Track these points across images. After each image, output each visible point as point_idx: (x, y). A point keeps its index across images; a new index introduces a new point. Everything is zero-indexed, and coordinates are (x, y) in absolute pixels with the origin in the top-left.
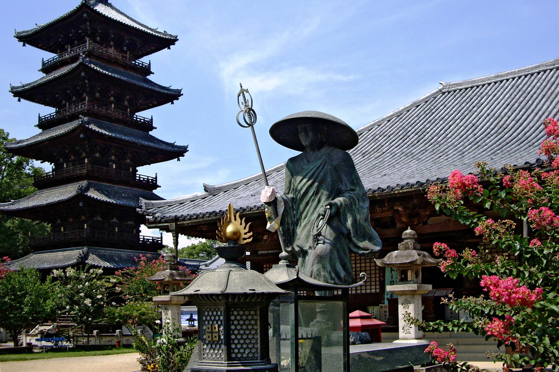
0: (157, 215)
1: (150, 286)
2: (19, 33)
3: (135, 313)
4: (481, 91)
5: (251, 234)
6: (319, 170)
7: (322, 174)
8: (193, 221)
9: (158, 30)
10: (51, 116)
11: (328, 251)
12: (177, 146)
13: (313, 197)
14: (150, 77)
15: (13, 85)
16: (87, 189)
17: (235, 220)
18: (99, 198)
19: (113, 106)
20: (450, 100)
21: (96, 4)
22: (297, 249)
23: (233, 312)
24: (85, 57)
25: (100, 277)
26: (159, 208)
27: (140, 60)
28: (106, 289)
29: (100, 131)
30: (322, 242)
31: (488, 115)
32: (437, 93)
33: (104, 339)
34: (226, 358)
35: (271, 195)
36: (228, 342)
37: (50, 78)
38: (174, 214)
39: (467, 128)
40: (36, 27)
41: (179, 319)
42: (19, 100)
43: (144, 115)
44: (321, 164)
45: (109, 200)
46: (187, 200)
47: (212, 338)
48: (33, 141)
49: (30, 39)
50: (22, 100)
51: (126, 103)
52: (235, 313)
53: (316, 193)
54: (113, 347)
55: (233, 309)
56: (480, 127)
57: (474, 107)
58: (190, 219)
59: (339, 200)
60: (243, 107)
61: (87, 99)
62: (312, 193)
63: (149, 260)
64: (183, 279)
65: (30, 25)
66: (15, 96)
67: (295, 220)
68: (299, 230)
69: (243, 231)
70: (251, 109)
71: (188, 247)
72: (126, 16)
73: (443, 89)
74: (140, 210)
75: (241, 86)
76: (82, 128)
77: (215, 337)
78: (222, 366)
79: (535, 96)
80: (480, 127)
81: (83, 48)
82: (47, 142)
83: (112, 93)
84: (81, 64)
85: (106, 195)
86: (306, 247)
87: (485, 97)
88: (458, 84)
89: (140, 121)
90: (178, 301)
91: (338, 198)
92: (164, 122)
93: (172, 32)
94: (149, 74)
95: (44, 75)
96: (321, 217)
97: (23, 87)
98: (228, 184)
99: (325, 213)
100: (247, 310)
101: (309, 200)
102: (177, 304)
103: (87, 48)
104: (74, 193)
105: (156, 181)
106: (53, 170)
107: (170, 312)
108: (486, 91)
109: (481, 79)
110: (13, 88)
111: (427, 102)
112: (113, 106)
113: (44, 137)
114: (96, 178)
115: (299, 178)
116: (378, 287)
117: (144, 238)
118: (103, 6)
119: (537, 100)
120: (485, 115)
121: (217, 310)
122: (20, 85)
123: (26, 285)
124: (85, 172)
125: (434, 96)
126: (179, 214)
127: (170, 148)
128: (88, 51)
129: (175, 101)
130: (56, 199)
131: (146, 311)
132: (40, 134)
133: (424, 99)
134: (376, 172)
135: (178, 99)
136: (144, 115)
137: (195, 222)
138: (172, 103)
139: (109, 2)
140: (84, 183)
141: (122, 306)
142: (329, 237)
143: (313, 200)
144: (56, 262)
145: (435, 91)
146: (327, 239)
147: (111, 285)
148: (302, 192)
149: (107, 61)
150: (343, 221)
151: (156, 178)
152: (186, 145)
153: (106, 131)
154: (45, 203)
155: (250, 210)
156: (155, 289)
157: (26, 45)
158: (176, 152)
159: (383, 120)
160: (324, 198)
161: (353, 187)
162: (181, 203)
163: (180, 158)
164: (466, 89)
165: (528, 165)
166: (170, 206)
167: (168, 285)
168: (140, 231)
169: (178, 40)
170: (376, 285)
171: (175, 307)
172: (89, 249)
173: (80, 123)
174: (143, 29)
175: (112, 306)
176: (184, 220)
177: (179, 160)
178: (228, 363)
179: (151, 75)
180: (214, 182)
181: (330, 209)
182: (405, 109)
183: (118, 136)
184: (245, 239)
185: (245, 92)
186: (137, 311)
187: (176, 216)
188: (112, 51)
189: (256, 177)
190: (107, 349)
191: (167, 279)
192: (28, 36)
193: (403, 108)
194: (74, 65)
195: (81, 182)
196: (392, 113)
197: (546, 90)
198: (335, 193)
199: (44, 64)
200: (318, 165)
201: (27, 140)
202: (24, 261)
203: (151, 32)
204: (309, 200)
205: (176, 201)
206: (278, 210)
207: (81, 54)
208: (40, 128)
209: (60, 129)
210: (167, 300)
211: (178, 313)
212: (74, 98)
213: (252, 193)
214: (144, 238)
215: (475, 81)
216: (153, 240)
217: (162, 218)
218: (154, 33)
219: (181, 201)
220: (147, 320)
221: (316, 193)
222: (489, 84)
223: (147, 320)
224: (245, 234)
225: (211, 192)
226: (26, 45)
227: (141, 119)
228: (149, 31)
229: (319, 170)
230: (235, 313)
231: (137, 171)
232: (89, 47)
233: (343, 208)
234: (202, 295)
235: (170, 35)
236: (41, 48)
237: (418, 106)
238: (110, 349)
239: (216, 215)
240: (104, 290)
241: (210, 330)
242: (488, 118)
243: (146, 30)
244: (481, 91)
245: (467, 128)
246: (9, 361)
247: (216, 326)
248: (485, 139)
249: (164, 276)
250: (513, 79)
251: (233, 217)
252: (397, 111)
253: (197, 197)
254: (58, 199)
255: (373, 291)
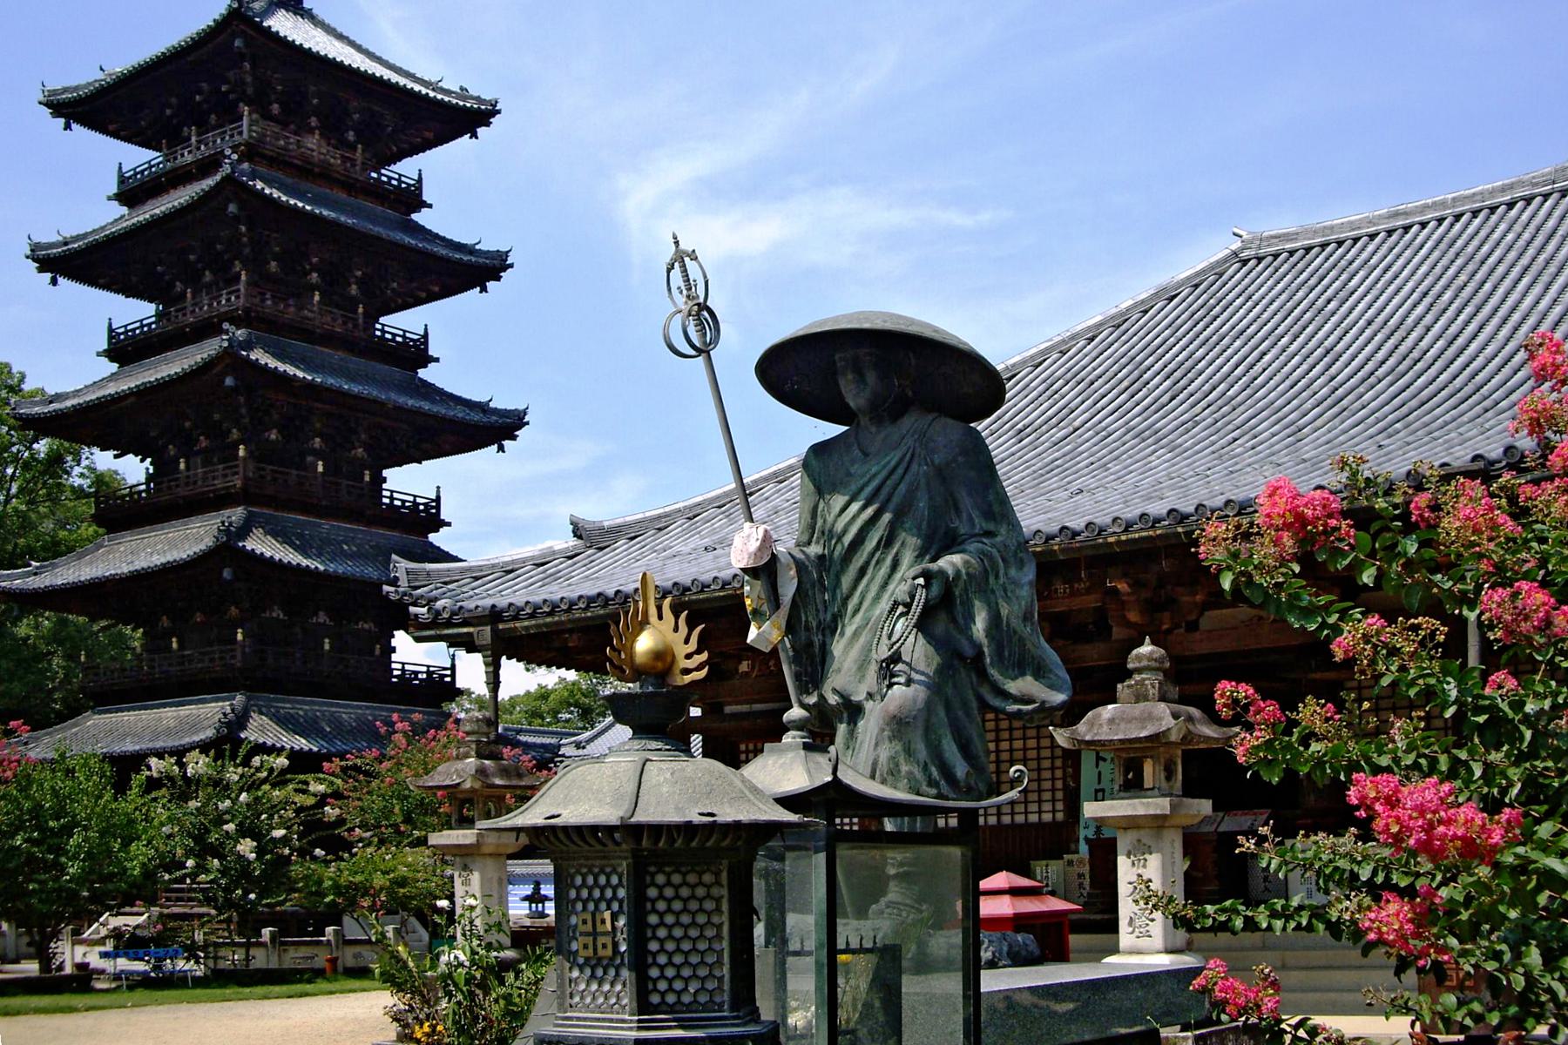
0: (439, 604)
1: (422, 803)
2: (54, 92)
3: (379, 880)
4: (1349, 256)
5: (704, 656)
6: (896, 477)
7: (903, 488)
8: (541, 621)
9: (443, 85)
10: (142, 326)
11: (920, 704)
12: (496, 411)
13: (878, 555)
14: (421, 217)
15: (36, 239)
16: (244, 531)
17: (660, 617)
18: (277, 557)
19: (317, 298)
20: (1263, 282)
21: (268, 12)
22: (833, 699)
23: (653, 875)
24: (240, 161)
25: (279, 779)
26: (446, 583)
27: (393, 167)
28: (298, 811)
29: (282, 367)
30: (902, 680)
31: (1369, 323)
32: (1225, 260)
33: (292, 952)
34: (635, 1004)
35: (760, 549)
36: (640, 961)
37: (141, 218)
38: (488, 602)
39: (1310, 361)
40: (101, 76)
41: (501, 897)
42: (54, 282)
43: (403, 322)
44: (901, 460)
45: (305, 562)
46: (524, 561)
47: (595, 950)
48: (94, 397)
49: (84, 109)
50: (60, 280)
51: (354, 289)
52: (660, 879)
53: (887, 542)
54: (316, 974)
55: (652, 869)
56: (1345, 357)
57: (1329, 301)
58: (532, 616)
59: (951, 562)
60: (681, 300)
61: (243, 278)
62: (874, 543)
63: (418, 731)
64: (514, 782)
65: (85, 70)
66: (41, 270)
67: (829, 617)
68: (837, 647)
69: (681, 650)
70: (703, 307)
71: (528, 693)
72: (352, 44)
73: (1243, 249)
74: (392, 589)
75: (677, 243)
76: (230, 359)
77: (604, 946)
78: (622, 1029)
79: (1501, 269)
80: (1345, 357)
81: (232, 136)
82: (132, 399)
83: (315, 260)
84: (227, 179)
85: (296, 548)
86: (857, 693)
87: (1362, 273)
88: (1284, 235)
89: (393, 340)
90: (498, 846)
91: (948, 557)
92: (460, 342)
93: (482, 90)
94: (417, 209)
95: (125, 210)
96: (901, 609)
97: (66, 244)
98: (640, 516)
99: (912, 597)
100: (693, 871)
101: (867, 563)
102: (495, 855)
103: (245, 135)
104: (207, 542)
105: (438, 507)
106: (150, 478)
107: (476, 877)
108: (1364, 255)
109: (1351, 223)
110: (35, 248)
111: (1196, 286)
112: (317, 298)
113: (125, 385)
114: (269, 500)
115: (839, 501)
116: (1060, 806)
117: (403, 670)
118: (290, 16)
119: (1507, 282)
120: (1362, 322)
121: (608, 870)
122: (55, 238)
123: (72, 801)
124: (239, 483)
125: (1218, 270)
126: (502, 602)
127: (476, 417)
128: (247, 144)
129: (490, 285)
130: (158, 560)
131: (410, 875)
132: (113, 377)
133: (1189, 278)
134: (1053, 482)
135: (498, 279)
136: (403, 322)
137: (546, 625)
138: (484, 289)
139: (307, 5)
140: (236, 514)
141: (343, 860)
142: (922, 667)
143: (878, 562)
144: (157, 737)
145: (1220, 255)
146: (917, 672)
147: (311, 801)
148: (847, 539)
149: (301, 172)
150: (961, 621)
151: (438, 500)
152: (521, 407)
153: (298, 367)
154: (125, 569)
155: (702, 591)
156: (435, 812)
157: (74, 126)
158: (493, 428)
159: (1073, 337)
160: (907, 557)
161: (991, 527)
162: (509, 570)
163: (506, 443)
164: (1308, 250)
165: (1481, 464)
166: (476, 579)
167: (470, 801)
168: (394, 650)
169: (499, 112)
170: (1054, 801)
171: (490, 862)
172: (249, 699)
173: (226, 344)
174: (402, 81)
175: (314, 859)
176: (516, 618)
177: (501, 449)
178: (639, 1021)
179: (424, 210)
180: (601, 511)
181: (927, 586)
182: (1136, 305)
183: (331, 381)
184: (687, 671)
185: (687, 259)
186: (385, 873)
187: (494, 606)
188: (313, 143)
189: (718, 497)
190: (300, 981)
191: (468, 785)
192: (79, 102)
193: (1130, 302)
194: (208, 183)
195: (227, 512)
196: (1099, 318)
197: (1531, 252)
198: (939, 541)
199: (122, 179)
200: (893, 463)
201: (77, 393)
202: (68, 733)
203: (424, 91)
204: (867, 563)
205: (493, 566)
206: (780, 591)
207: (228, 152)
208: (112, 360)
209: (168, 362)
210: (468, 842)
211: (500, 881)
212: (208, 276)
213: (707, 541)
214: (403, 670)
215: (1332, 228)
216: (429, 673)
217: (453, 613)
218: (432, 94)
219: (507, 563)
220: (413, 898)
221: (887, 542)
222: (1372, 237)
223: (413, 898)
224: (688, 656)
225: (592, 538)
226: (74, 126)
227: (394, 335)
228: (417, 88)
229: (896, 477)
230: (660, 879)
231: (384, 480)
232: (250, 131)
233: (961, 584)
234: (566, 829)
235: (478, 99)
236: (115, 135)
237: (1171, 299)
238: (309, 982)
239: (606, 605)
240: (291, 814)
241: (589, 927)
242: (1368, 332)
243: (410, 85)
244: (1349, 256)
245: (1310, 361)
246: (26, 1013)
247: (607, 915)
248: (1361, 389)
249: (459, 776)
250: (1440, 221)
251: (653, 611)
252: (1114, 311)
253: (554, 553)
254: (163, 560)
255: (1047, 817)
